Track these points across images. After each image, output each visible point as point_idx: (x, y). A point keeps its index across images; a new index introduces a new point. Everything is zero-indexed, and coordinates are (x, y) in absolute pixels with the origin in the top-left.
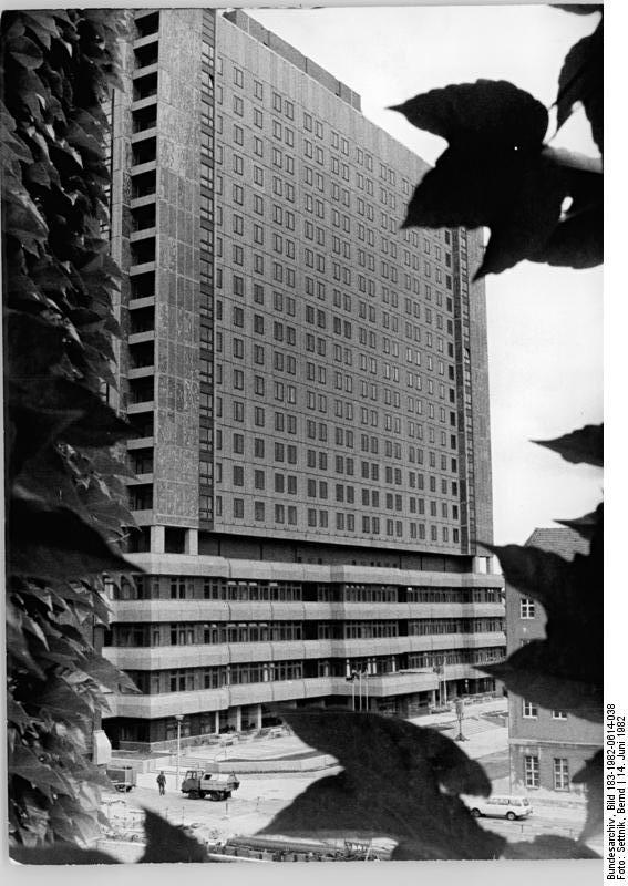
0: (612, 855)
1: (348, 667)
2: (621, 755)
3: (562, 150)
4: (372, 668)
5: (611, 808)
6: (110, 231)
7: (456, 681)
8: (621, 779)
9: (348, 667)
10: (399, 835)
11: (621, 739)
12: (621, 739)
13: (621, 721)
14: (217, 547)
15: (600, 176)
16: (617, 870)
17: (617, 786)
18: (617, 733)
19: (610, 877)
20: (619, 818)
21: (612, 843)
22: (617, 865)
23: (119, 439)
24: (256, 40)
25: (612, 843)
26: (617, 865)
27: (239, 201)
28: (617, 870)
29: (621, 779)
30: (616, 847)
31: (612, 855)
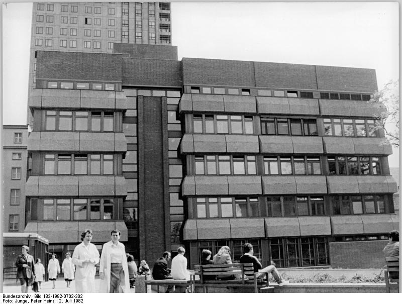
0: (14, 297)
2: (67, 301)
6: (234, 217)
7: (300, 237)
8: (59, 301)
10: (171, 46)
11: (55, 301)
12: (42, 301)
13: (81, 301)
14: (178, 191)
16: (7, 299)
17: (55, 299)
18: (76, 299)
19: (4, 296)
20: (29, 300)
21: (20, 297)
22: (10, 299)
23: (42, 236)
25: (20, 297)
26: (10, 299)
28: (7, 299)
30: (5, 298)
31: (14, 297)
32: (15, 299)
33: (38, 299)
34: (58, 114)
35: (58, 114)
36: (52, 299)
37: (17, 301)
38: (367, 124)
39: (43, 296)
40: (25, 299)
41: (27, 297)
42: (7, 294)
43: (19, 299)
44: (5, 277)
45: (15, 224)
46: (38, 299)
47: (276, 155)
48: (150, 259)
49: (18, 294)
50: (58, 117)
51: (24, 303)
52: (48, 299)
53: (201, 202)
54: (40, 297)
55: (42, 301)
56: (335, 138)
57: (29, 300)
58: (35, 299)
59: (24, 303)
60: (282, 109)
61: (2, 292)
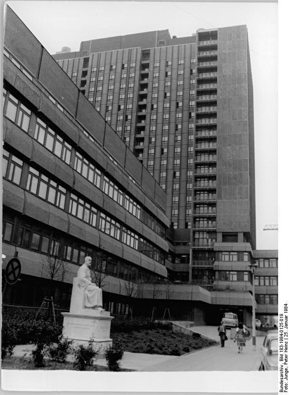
0: (282, 381)
1: (53, 303)
3: (57, 53)
4: (220, 237)
5: (281, 360)
9: (53, 303)
11: (286, 341)
12: (286, 314)
15: (278, 251)
16: (284, 388)
17: (284, 341)
19: (281, 391)
20: (285, 367)
21: (282, 376)
22: (284, 385)
24: (223, 191)
25: (282, 376)
26: (284, 385)
27: (10, 178)
28: (284, 388)
29: (286, 337)
30: (283, 390)
32: (285, 380)
33: (284, 358)
34: (229, 253)
35: (229, 253)
36: (284, 344)
37: (286, 378)
38: (10, 161)
39: (281, 353)
40: (284, 370)
41: (282, 369)
42: (280, 388)
43: (284, 377)
44: (263, 302)
45: (247, 171)
46: (284, 358)
47: (125, 116)
48: (32, 323)
49: (279, 377)
50: (230, 255)
51: (288, 372)
52: (284, 348)
53: (150, 209)
54: (282, 355)
55: (286, 314)
56: (44, 148)
57: (285, 367)
58: (284, 361)
59: (288, 372)
60: (156, 345)
61: (277, 393)
